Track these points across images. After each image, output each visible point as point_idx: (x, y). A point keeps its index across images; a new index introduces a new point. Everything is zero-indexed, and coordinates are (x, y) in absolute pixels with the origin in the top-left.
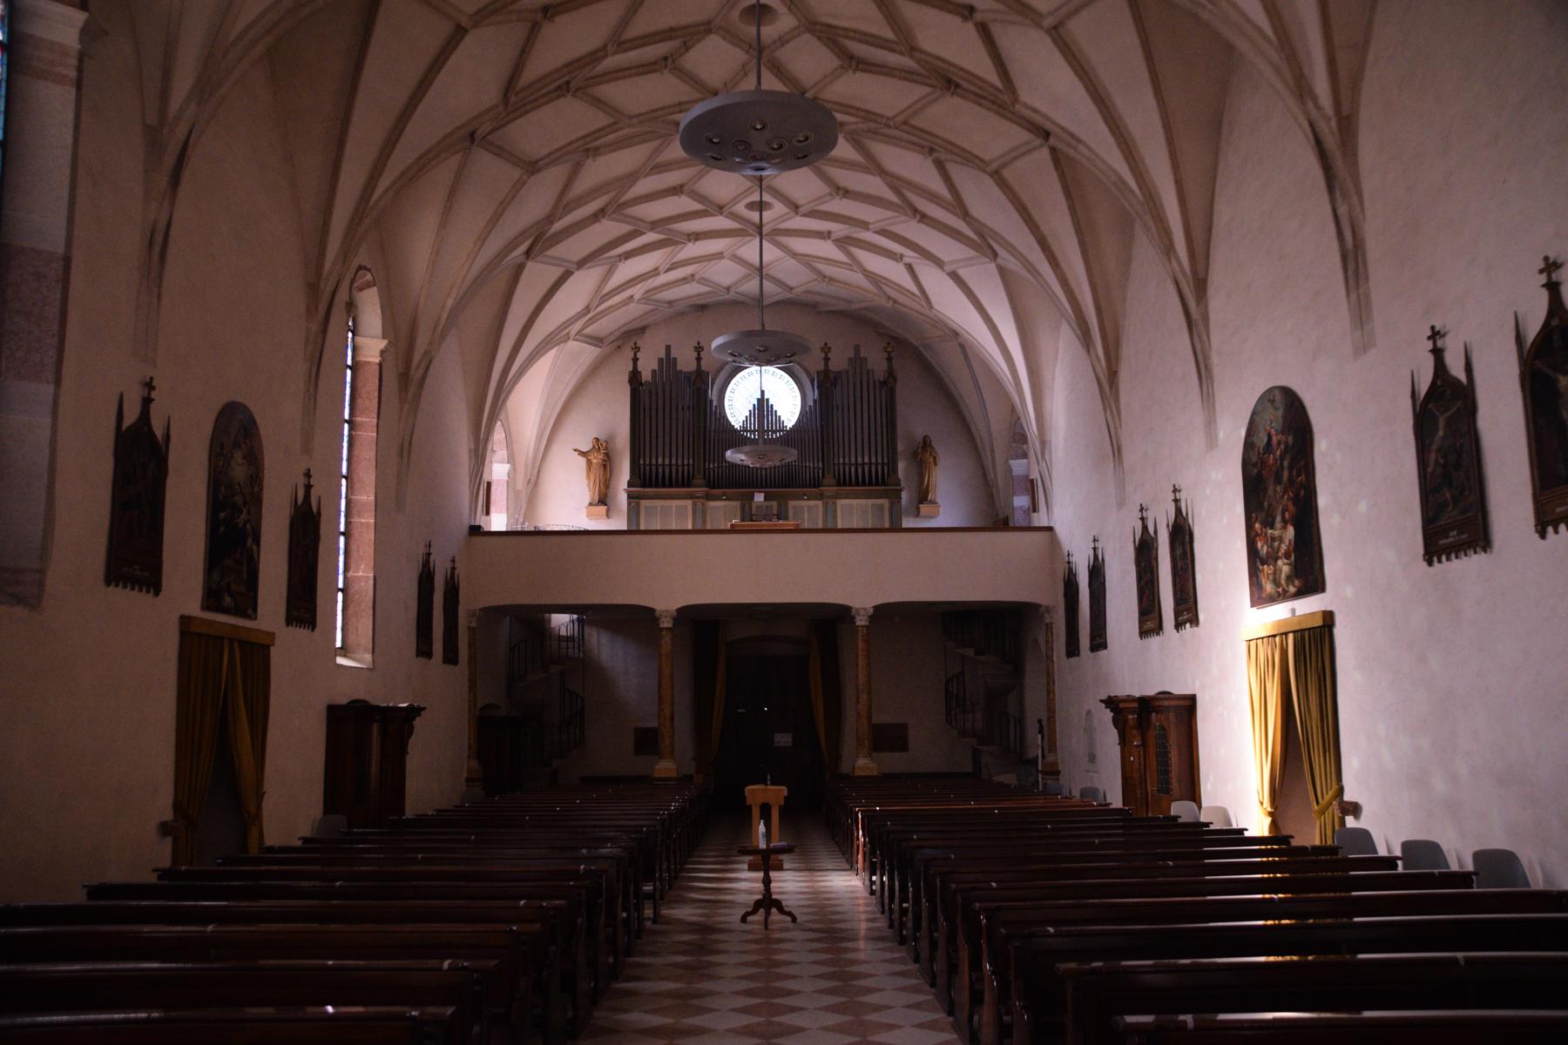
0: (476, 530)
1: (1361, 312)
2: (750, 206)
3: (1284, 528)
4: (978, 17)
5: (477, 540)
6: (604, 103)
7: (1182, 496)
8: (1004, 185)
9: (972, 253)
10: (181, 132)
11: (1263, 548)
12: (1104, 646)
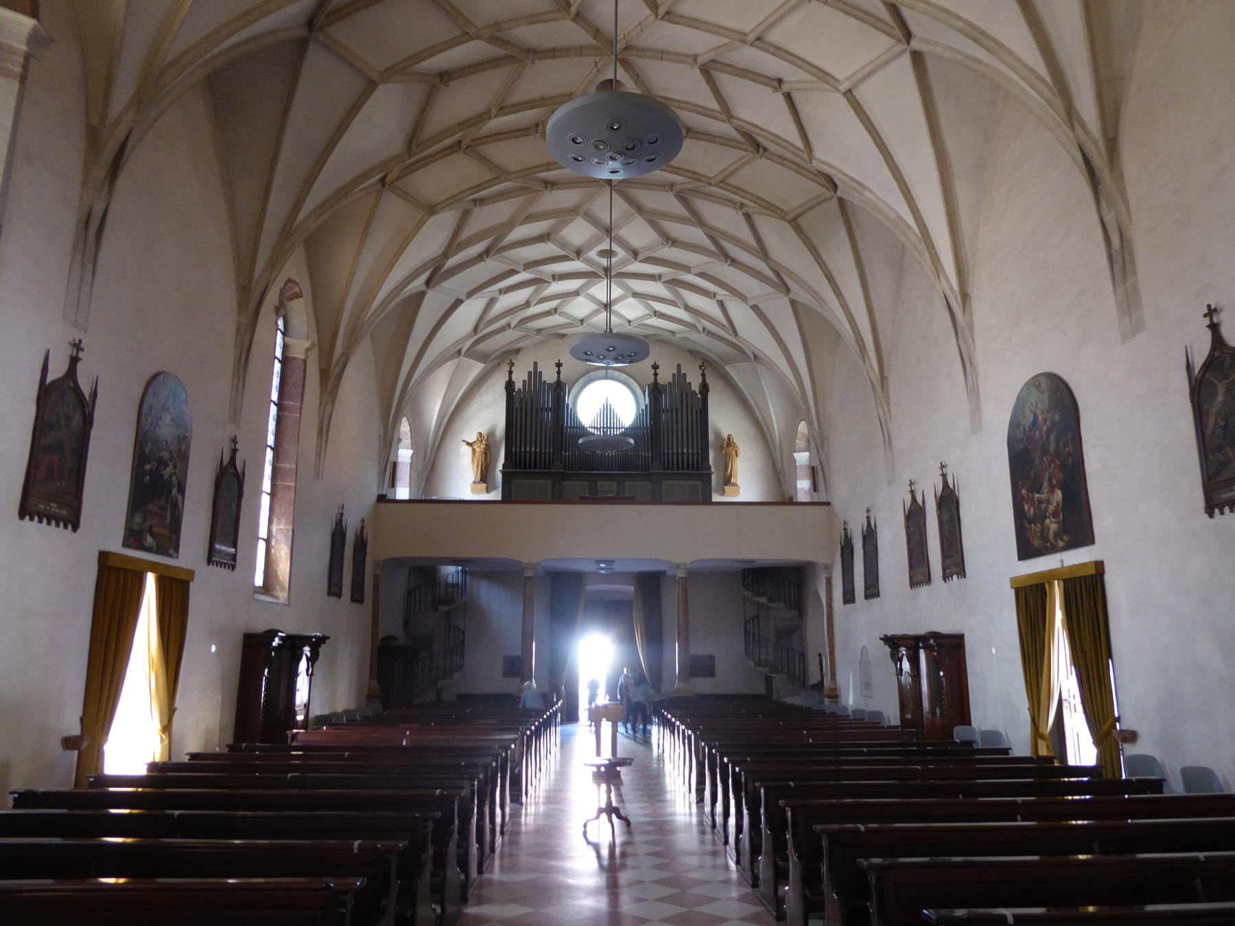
0: (382, 499)
1: (1129, 302)
2: (603, 253)
3: (1052, 491)
4: (786, 87)
5: (385, 507)
6: (489, 161)
7: (872, 515)
8: (799, 231)
9: (772, 290)
10: (120, 134)
11: (1030, 510)
12: (877, 595)
